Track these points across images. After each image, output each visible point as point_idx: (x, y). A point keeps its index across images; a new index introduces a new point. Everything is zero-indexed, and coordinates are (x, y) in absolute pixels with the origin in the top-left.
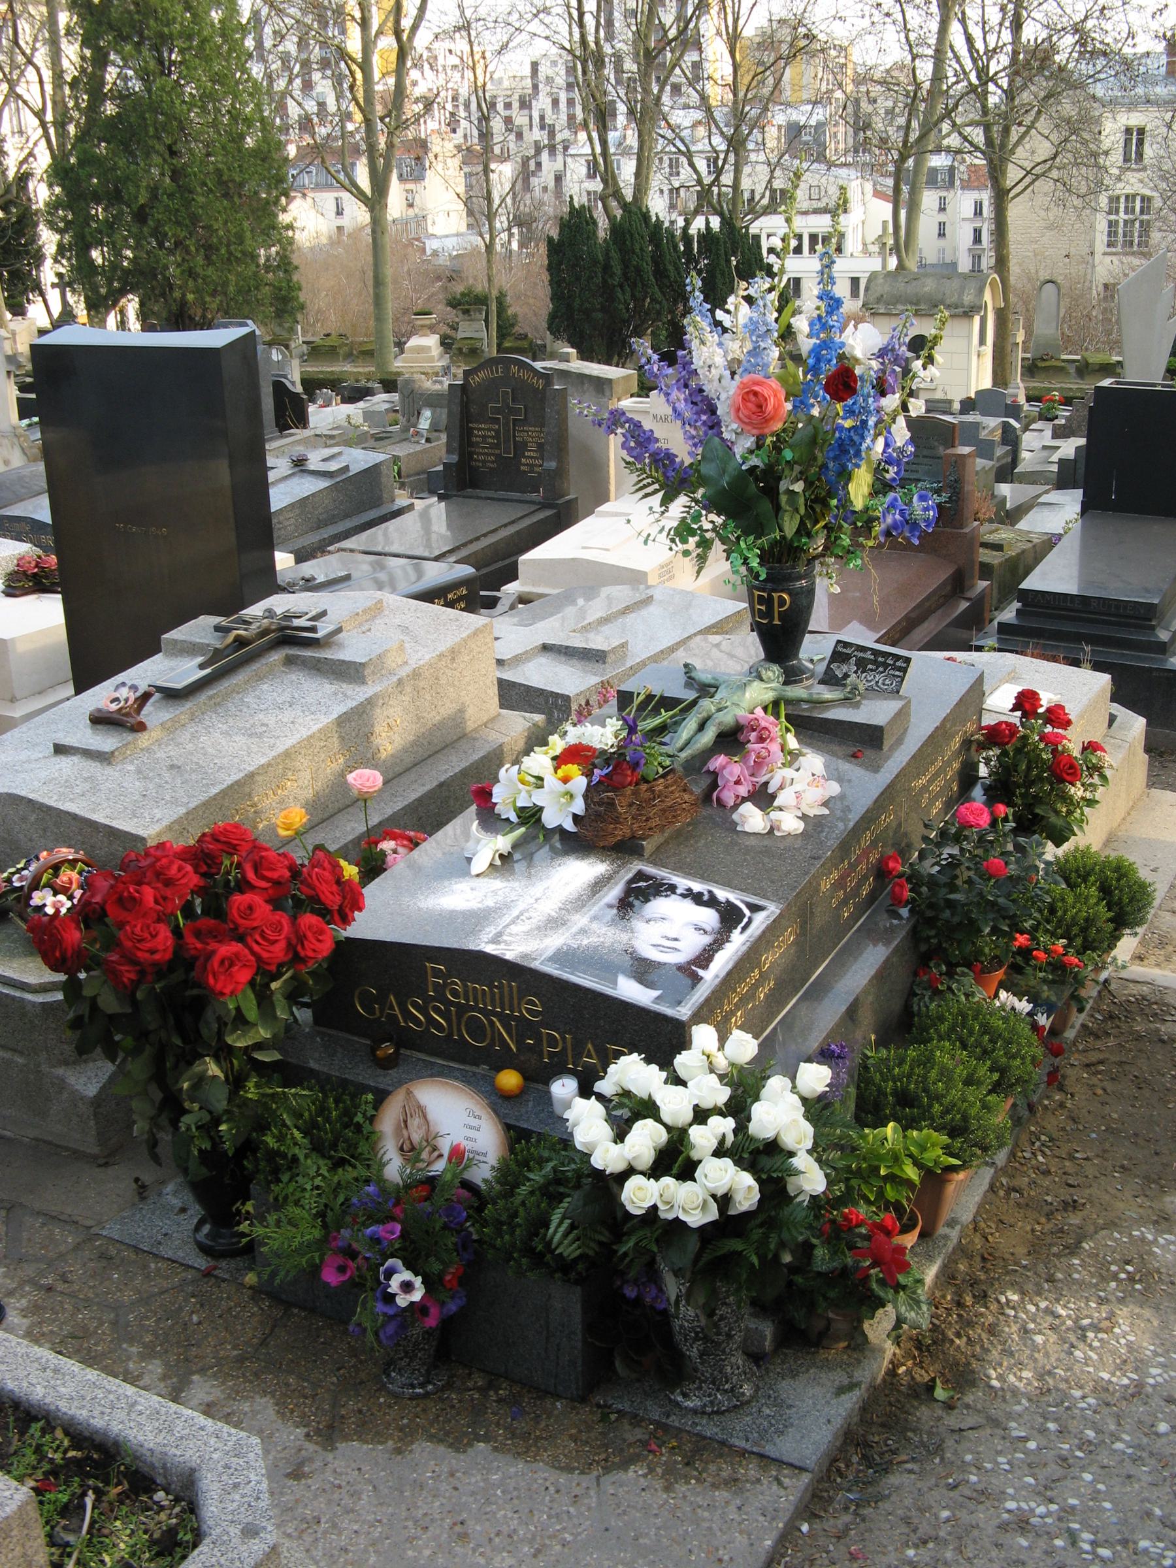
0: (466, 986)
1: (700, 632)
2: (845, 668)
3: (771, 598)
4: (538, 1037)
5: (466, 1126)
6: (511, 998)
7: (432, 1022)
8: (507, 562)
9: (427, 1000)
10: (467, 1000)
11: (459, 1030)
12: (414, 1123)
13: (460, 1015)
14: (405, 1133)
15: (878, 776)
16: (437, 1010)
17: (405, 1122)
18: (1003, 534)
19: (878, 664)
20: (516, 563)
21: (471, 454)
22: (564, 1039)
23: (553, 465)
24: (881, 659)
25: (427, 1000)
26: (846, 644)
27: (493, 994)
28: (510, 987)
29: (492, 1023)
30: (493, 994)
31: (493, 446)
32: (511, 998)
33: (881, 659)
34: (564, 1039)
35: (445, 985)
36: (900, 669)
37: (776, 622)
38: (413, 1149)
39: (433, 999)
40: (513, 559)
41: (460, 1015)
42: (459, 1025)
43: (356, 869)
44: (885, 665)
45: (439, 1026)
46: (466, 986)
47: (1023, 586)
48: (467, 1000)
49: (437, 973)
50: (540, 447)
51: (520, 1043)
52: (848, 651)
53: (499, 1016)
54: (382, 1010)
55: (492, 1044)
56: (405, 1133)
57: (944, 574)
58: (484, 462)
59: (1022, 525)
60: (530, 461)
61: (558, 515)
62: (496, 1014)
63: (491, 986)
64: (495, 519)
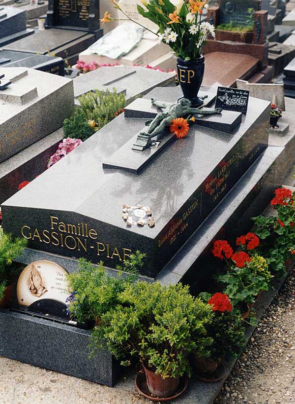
0: (66, 225)
1: (158, 85)
2: (224, 98)
3: (187, 72)
4: (96, 245)
5: (57, 284)
6: (85, 230)
7: (52, 240)
8: (74, 56)
9: (51, 231)
10: (67, 231)
11: (64, 243)
12: (35, 278)
13: (64, 238)
14: (32, 282)
15: (229, 144)
16: (54, 234)
17: (32, 278)
18: (278, 47)
19: (237, 95)
20: (78, 56)
21: (59, 10)
22: (106, 246)
23: (93, 16)
24: (237, 93)
25: (51, 231)
26: (222, 88)
27: (77, 229)
28: (85, 226)
29: (77, 240)
30: (77, 229)
31: (67, 7)
32: (85, 230)
33: (237, 93)
34: (106, 246)
35: (58, 225)
36: (245, 96)
37: (189, 82)
38: (35, 288)
39: (53, 231)
40: (77, 55)
41: (64, 238)
42: (64, 240)
43: (75, 103)
44: (240, 95)
45: (56, 242)
46: (66, 225)
47: (285, 69)
48: (67, 231)
49: (54, 220)
50: (88, 8)
51: (88, 247)
52: (224, 91)
53: (79, 237)
54: (32, 236)
55: (77, 248)
56: (32, 282)
57: (254, 63)
58: (64, 14)
59: (287, 43)
60: (83, 14)
61: (95, 36)
62: (79, 237)
63: (76, 225)
64: (68, 37)
